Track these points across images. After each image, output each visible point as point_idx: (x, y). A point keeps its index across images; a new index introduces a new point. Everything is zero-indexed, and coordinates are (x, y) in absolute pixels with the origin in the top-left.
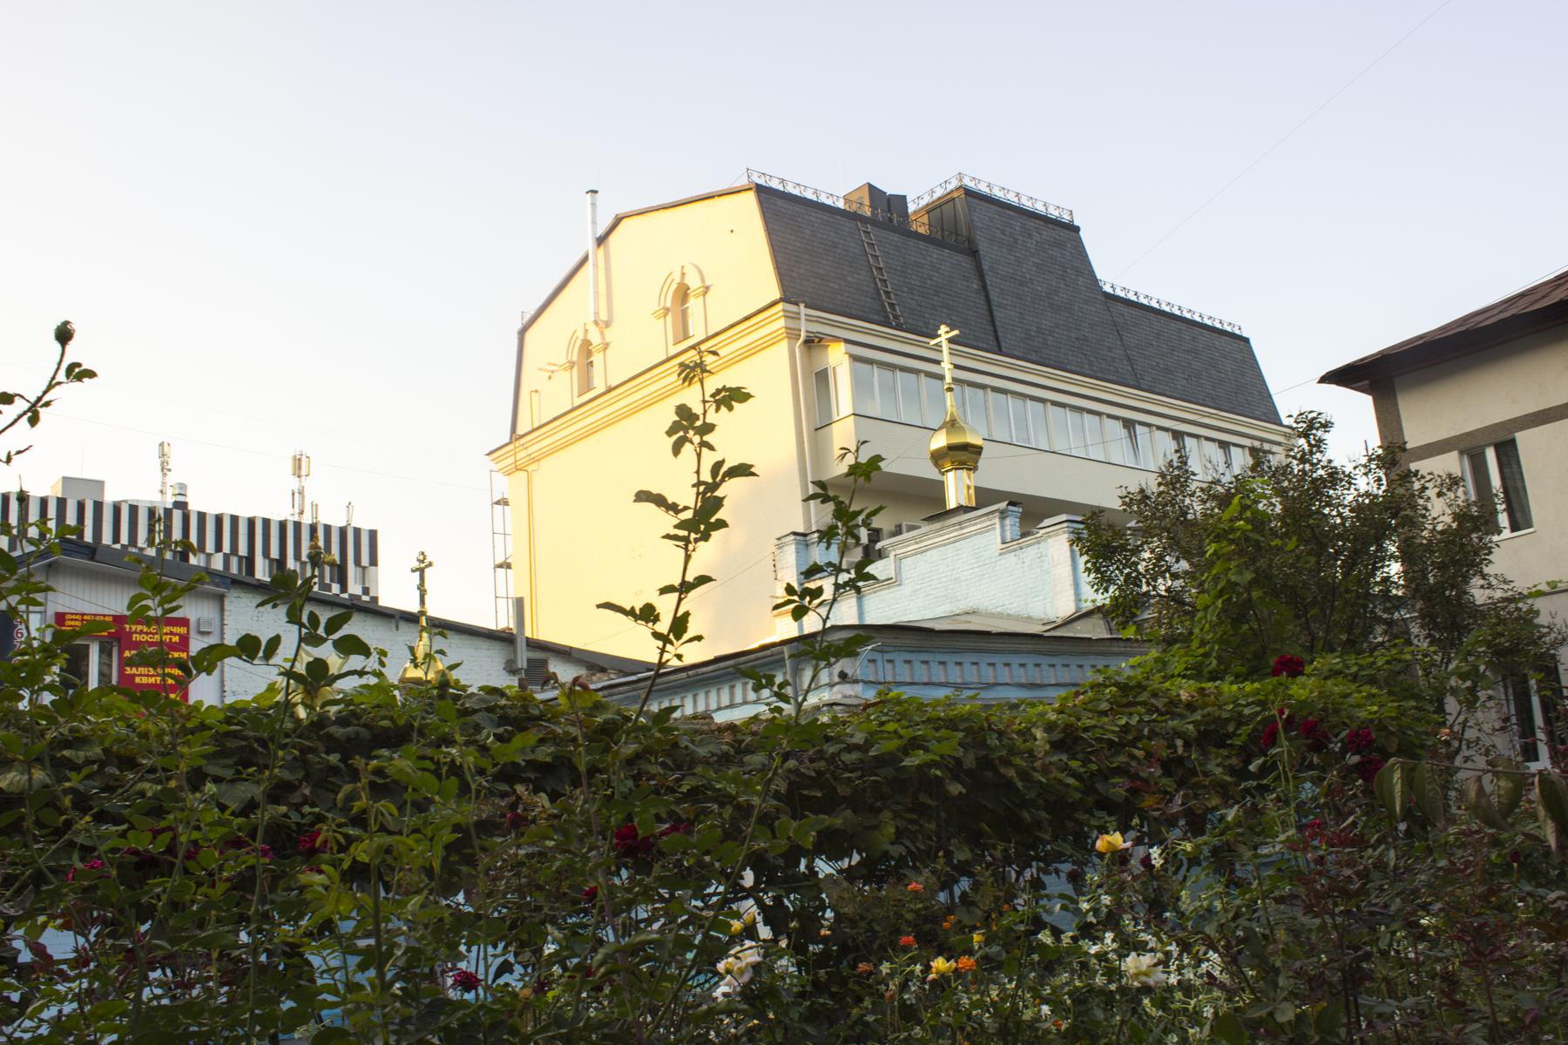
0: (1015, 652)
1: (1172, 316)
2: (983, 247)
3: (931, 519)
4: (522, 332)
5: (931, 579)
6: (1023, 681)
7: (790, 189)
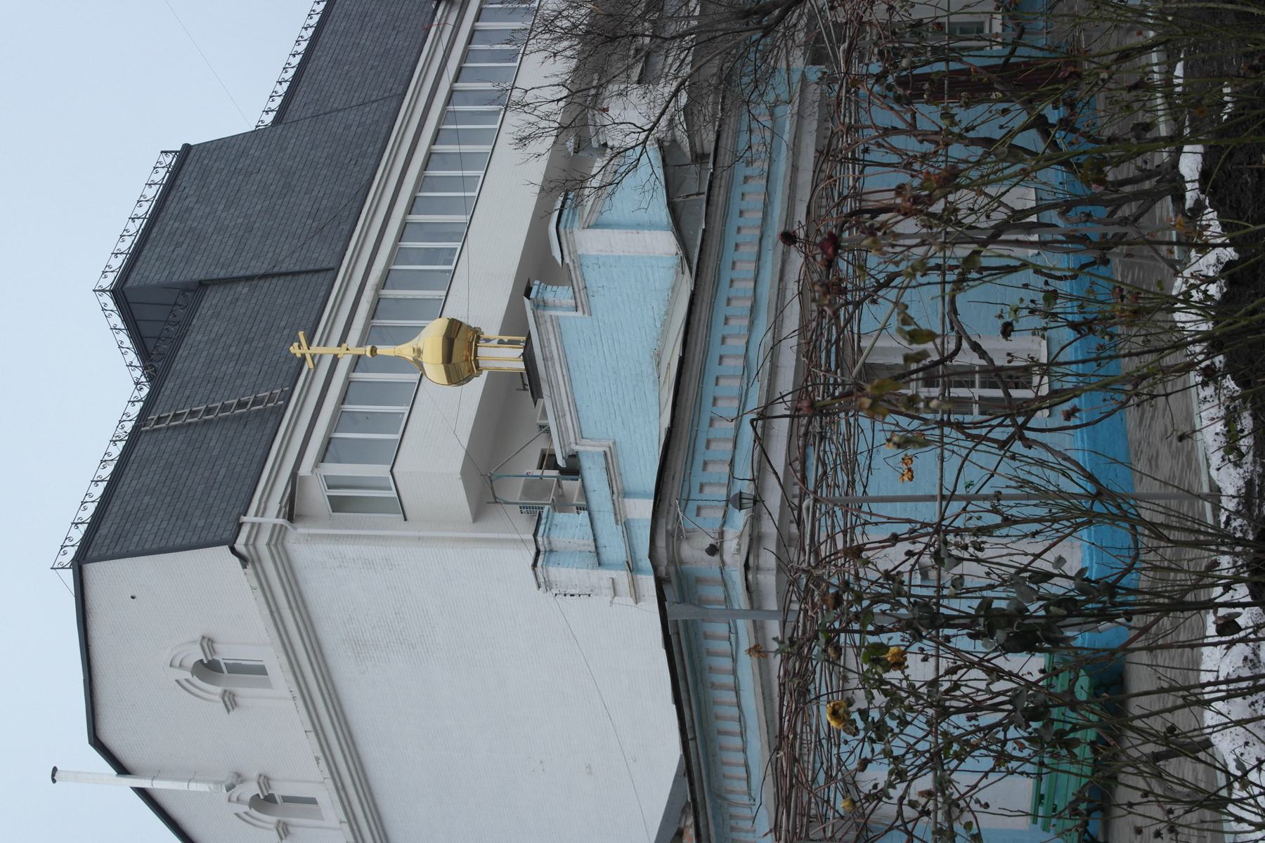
0: (709, 327)
1: (314, 40)
2: (196, 273)
3: (536, 393)
4: (97, 742)
5: (614, 400)
6: (746, 322)
7: (87, 515)
